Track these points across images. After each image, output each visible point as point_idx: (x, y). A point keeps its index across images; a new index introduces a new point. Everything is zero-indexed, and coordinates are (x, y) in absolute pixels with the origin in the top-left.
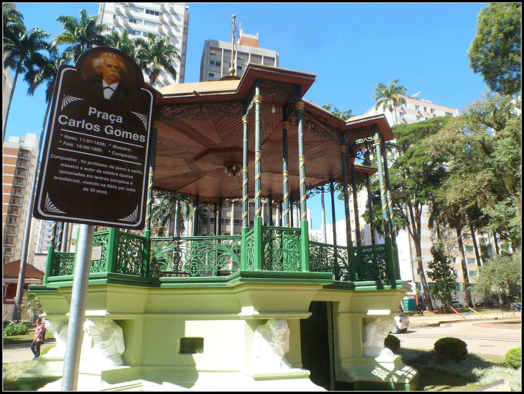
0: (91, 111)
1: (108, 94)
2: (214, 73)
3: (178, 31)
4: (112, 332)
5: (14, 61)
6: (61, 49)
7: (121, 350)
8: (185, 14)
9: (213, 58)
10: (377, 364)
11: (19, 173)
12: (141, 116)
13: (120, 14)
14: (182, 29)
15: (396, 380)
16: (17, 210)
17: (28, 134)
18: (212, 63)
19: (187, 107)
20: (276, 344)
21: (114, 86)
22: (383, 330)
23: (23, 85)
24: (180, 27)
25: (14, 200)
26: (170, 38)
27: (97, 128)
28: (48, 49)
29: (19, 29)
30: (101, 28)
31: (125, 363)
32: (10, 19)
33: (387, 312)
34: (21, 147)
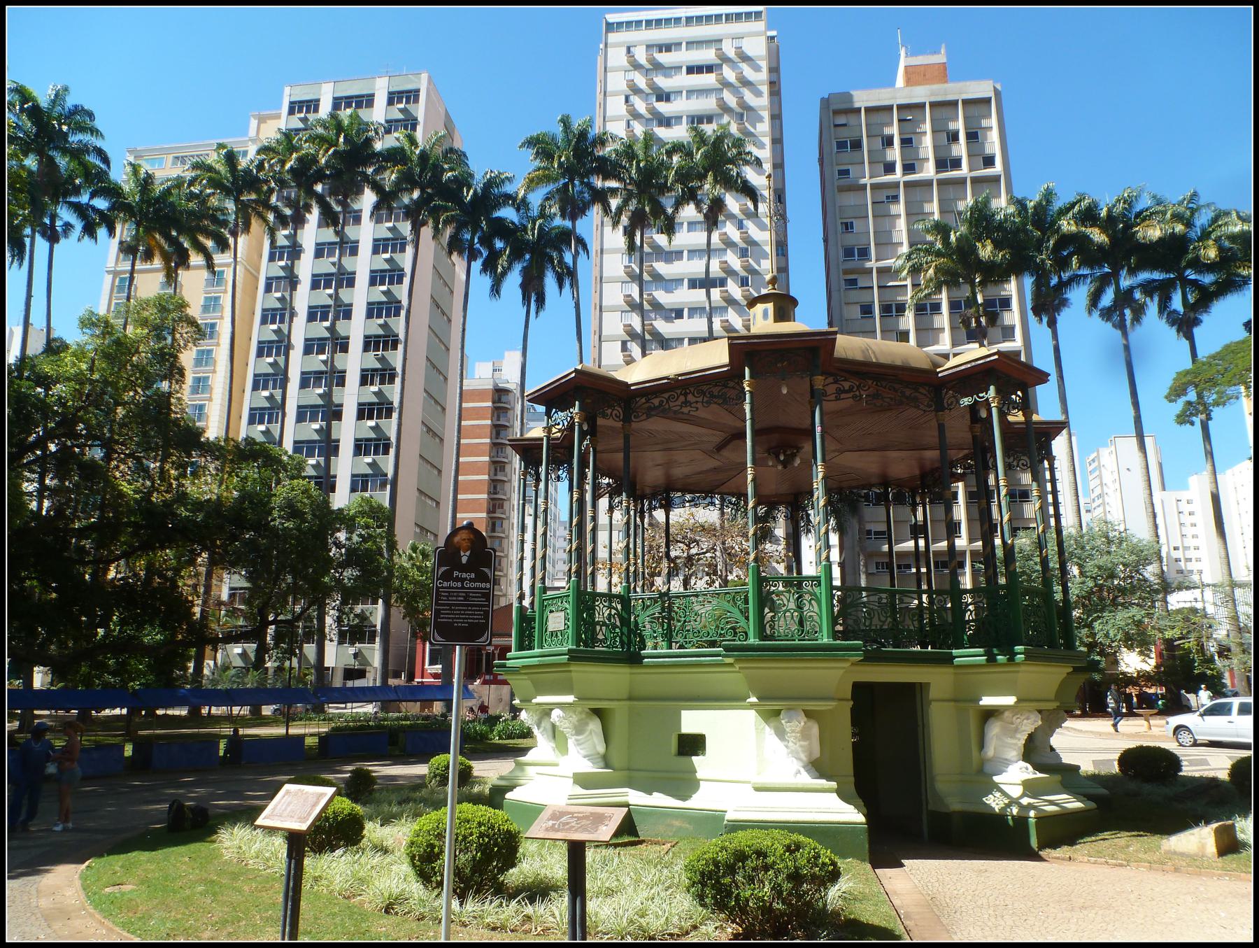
0: (456, 574)
1: (464, 560)
2: (850, 167)
3: (758, 94)
4: (587, 724)
5: (461, 240)
6: (536, 199)
7: (601, 748)
8: (769, 50)
9: (845, 134)
10: (996, 787)
11: (498, 434)
12: (486, 570)
13: (636, 90)
14: (765, 89)
15: (1015, 811)
16: (502, 506)
17: (506, 354)
18: (841, 145)
19: (666, 395)
20: (791, 744)
21: (468, 553)
22: (1016, 730)
23: (482, 282)
24: (762, 83)
25: (495, 488)
26: (742, 115)
27: (459, 585)
28: (513, 205)
29: (464, 180)
30: (601, 141)
31: (607, 766)
32: (446, 166)
33: (1010, 700)
34: (496, 385)
